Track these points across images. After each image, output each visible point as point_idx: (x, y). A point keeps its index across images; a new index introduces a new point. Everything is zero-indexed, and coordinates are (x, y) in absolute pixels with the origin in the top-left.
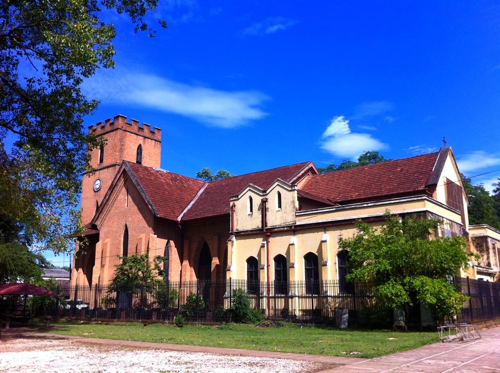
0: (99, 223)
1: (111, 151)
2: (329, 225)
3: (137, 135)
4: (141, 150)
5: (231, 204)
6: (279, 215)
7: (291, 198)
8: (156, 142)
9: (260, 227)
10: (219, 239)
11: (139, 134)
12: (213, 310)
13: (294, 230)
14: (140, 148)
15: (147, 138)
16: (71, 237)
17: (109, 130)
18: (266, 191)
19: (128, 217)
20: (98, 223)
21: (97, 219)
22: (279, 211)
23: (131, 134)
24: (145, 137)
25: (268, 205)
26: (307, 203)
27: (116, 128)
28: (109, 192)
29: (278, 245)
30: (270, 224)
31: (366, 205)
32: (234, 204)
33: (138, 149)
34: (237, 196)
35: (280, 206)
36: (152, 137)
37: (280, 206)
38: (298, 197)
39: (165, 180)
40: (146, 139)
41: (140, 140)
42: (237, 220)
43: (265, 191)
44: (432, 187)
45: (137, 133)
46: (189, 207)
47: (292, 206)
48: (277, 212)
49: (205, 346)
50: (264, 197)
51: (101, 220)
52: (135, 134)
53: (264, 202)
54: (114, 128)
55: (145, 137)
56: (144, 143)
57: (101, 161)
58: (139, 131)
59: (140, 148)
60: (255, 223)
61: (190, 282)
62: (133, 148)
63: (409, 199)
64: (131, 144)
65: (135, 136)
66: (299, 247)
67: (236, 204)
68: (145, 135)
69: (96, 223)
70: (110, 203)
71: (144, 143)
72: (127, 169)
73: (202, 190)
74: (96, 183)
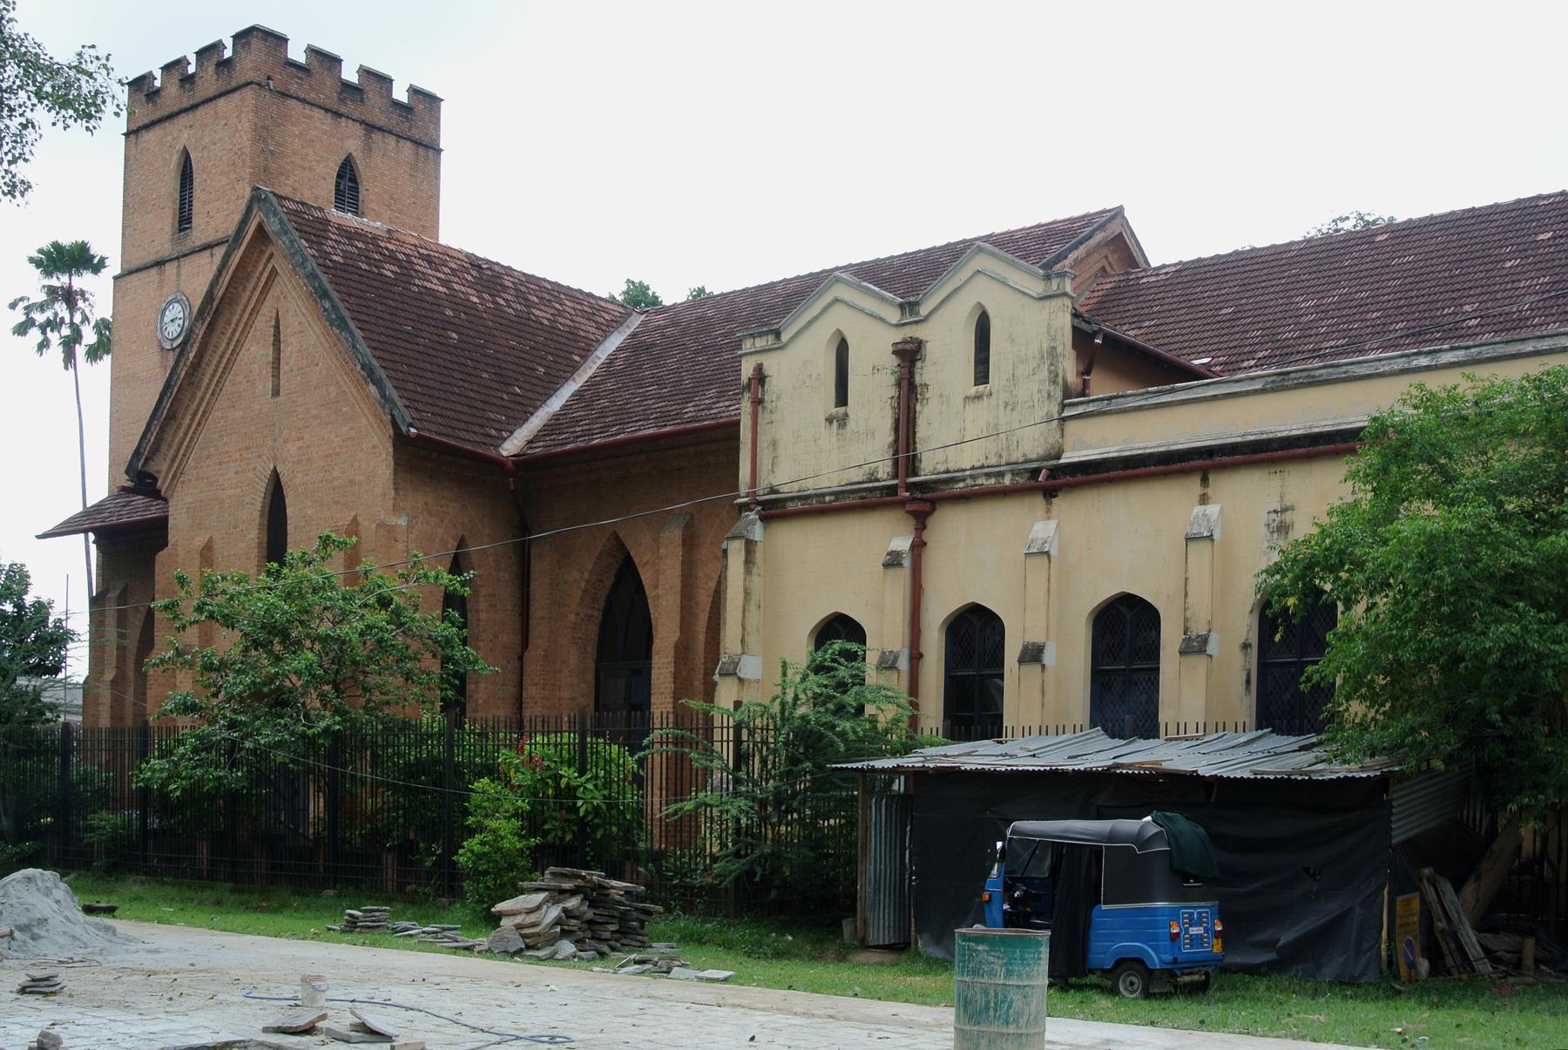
0: (164, 467)
1: (224, 181)
2: (1225, 459)
3: (338, 115)
4: (354, 180)
5: (747, 369)
6: (978, 418)
8: (421, 151)
9: (884, 470)
10: (690, 544)
11: (343, 110)
13: (1054, 480)
15: (380, 129)
17: (211, 92)
18: (917, 304)
19: (286, 441)
20: (160, 467)
21: (156, 449)
22: (978, 397)
23: (308, 110)
24: (370, 127)
25: (926, 373)
27: (242, 81)
28: (201, 331)
29: (979, 559)
30: (931, 464)
31: (1423, 361)
33: (339, 176)
34: (777, 334)
35: (982, 376)
36: (403, 128)
37: (982, 376)
38: (1074, 327)
39: (444, 283)
40: (377, 136)
41: (352, 141)
42: (774, 444)
45: (336, 107)
46: (556, 403)
47: (1044, 374)
48: (970, 407)
49: (244, 931)
51: (170, 455)
52: (327, 110)
53: (909, 354)
54: (234, 84)
55: (370, 127)
56: (368, 149)
57: (184, 220)
58: (342, 101)
60: (865, 452)
62: (320, 169)
64: (310, 151)
66: (1127, 544)
67: (767, 370)
68: (368, 118)
69: (152, 468)
70: (206, 381)
71: (368, 149)
72: (272, 226)
74: (169, 316)
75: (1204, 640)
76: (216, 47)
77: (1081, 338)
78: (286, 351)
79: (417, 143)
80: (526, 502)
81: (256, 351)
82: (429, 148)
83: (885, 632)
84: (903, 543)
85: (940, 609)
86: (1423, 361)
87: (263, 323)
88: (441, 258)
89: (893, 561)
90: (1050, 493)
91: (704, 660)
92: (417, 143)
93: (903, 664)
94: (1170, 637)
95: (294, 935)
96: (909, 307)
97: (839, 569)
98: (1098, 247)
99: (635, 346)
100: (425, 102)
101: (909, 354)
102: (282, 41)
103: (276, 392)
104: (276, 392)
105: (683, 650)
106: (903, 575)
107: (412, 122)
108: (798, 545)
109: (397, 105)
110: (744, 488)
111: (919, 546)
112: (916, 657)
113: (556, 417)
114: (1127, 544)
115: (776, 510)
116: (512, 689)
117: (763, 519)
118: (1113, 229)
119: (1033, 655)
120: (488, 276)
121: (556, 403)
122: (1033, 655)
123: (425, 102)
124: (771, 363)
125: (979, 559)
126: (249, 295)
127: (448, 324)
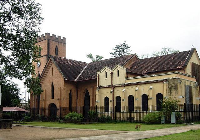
3: (55, 41)
7: (123, 72)
10: (93, 89)
12: (89, 117)
13: (124, 85)
14: (57, 47)
16: (8, 81)
17: (43, 40)
24: (59, 42)
26: (129, 73)
31: (154, 76)
32: (99, 74)
35: (118, 76)
43: (112, 69)
44: (184, 67)
46: (80, 75)
50: (112, 72)
55: (59, 42)
59: (57, 47)
61: (137, 106)
63: (171, 73)
65: (55, 42)
66: (131, 91)
72: (52, 59)
73: (85, 67)
75: (137, 99)
76: (43, 35)
77: (126, 72)
78: (53, 71)
79: (64, 43)
80: (78, 85)
81: (50, 71)
82: (65, 44)
83: (111, 99)
84: (112, 91)
85: (115, 96)
86: (154, 76)
87: (51, 68)
88: (67, 60)
89: (111, 92)
90: (124, 86)
91: (94, 101)
92: (64, 43)
93: (112, 101)
94: (134, 99)
95: (86, 123)
96: (112, 69)
97: (107, 93)
98: (133, 58)
99: (87, 68)
100: (65, 38)
101: (112, 74)
102: (50, 34)
103: (52, 75)
104: (52, 75)
105: (93, 99)
106: (112, 94)
107: (62, 41)
108: (104, 91)
109: (62, 39)
110: (98, 85)
111: (113, 91)
112: (113, 100)
113: (80, 77)
114: (131, 91)
115: (100, 87)
116: (76, 103)
117: (100, 88)
118: (135, 56)
119: (123, 100)
120: (73, 61)
121: (80, 75)
122: (123, 100)
123: (65, 38)
124: (100, 74)
125: (119, 92)
126: (50, 66)
127: (69, 67)
